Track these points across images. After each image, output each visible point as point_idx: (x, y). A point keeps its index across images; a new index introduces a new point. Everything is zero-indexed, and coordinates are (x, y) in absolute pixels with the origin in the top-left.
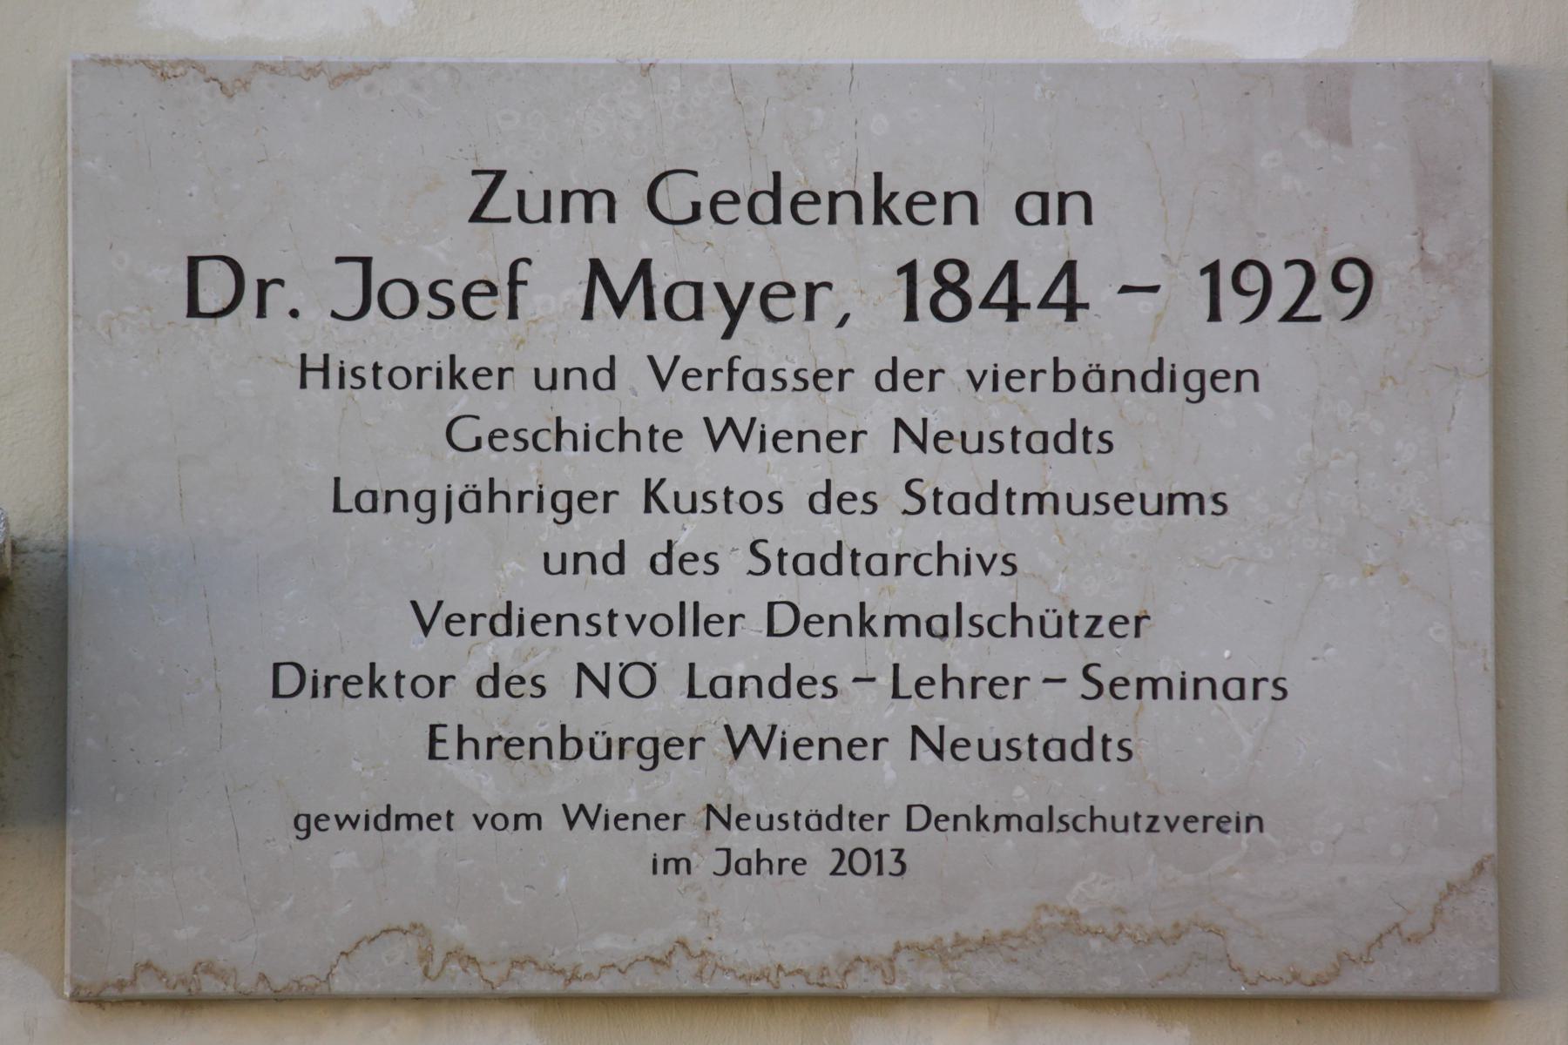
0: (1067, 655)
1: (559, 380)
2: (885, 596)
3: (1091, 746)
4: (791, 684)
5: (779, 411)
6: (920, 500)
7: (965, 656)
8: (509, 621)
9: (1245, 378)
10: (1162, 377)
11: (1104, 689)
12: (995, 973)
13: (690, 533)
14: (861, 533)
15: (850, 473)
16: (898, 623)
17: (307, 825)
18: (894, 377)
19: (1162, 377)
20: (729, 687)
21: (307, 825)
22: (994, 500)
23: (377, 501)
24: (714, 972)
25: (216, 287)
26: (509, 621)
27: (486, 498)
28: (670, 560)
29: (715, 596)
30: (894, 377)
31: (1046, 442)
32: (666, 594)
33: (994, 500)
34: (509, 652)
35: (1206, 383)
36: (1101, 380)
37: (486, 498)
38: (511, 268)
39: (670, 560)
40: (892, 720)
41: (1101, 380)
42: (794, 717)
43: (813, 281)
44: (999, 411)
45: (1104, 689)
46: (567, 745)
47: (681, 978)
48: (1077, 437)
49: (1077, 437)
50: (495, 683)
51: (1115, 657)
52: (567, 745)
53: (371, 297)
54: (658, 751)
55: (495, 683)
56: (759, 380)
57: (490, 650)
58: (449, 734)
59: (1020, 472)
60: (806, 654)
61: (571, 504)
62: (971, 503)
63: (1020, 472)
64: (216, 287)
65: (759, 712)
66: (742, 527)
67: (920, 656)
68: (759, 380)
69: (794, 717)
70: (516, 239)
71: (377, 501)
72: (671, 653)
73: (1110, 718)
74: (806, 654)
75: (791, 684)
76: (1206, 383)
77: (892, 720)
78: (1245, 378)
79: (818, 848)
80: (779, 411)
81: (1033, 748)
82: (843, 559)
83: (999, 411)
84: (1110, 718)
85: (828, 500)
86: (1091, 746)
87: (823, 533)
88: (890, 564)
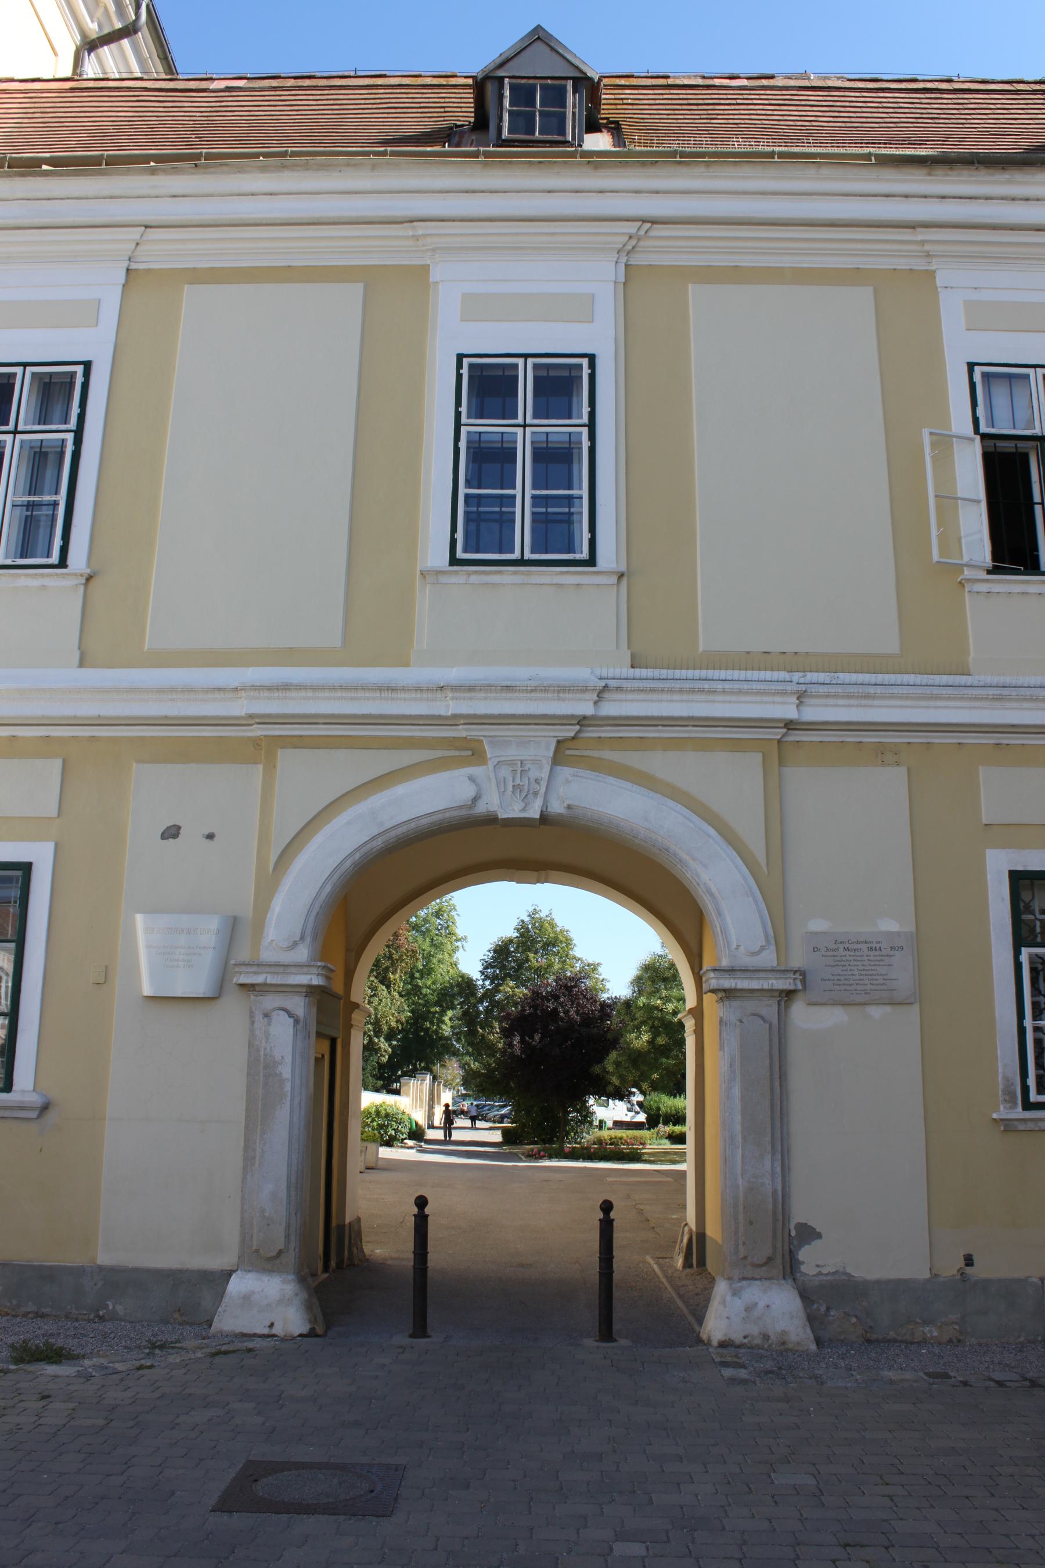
0: (881, 977)
1: (842, 956)
2: (867, 973)
3: (883, 984)
4: (861, 980)
5: (859, 959)
6: (870, 965)
7: (874, 977)
8: (839, 975)
9: (894, 955)
10: (888, 956)
11: (884, 980)
12: (877, 1002)
13: (852, 968)
14: (866, 968)
15: (864, 963)
16: (869, 975)
17: (824, 991)
18: (867, 956)
19: (888, 956)
20: (856, 980)
21: (824, 991)
22: (875, 965)
23: (828, 966)
24: (986, 1476)
25: (816, 949)
26: (839, 975)
27: (837, 965)
28: (851, 970)
29: (854, 973)
30: (867, 956)
31: (879, 961)
32: (850, 973)
33: (875, 965)
34: (839, 977)
35: (891, 956)
36: (883, 956)
37: (837, 965)
38: (168, 827)
39: (851, 970)
40: (868, 982)
41: (883, 956)
42: (861, 982)
43: (595, 960)
44: (876, 958)
45: (884, 980)
46: (844, 985)
47: (853, 1003)
48: (881, 960)
49: (881, 960)
50: (838, 980)
51: (885, 977)
52: (844, 985)
53: (827, 950)
54: (851, 985)
55: (838, 980)
56: (857, 956)
57: (838, 977)
58: (727, 1474)
59: (877, 963)
60: (862, 977)
61: (843, 966)
62: (873, 966)
63: (877, 963)
64: (816, 949)
65: (858, 982)
66: (857, 967)
67: (870, 977)
68: (857, 956)
69: (861, 982)
70: (838, 945)
71: (828, 966)
72: (851, 977)
73: (885, 982)
74: (862, 977)
75: (861, 980)
76: (891, 956)
77: (868, 982)
78: (894, 955)
79: (863, 992)
80: (859, 959)
81: (877, 985)
82: (864, 970)
83: (876, 958)
84: (885, 982)
85: (863, 965)
86: (883, 984)
87: (862, 968)
88: (868, 970)
